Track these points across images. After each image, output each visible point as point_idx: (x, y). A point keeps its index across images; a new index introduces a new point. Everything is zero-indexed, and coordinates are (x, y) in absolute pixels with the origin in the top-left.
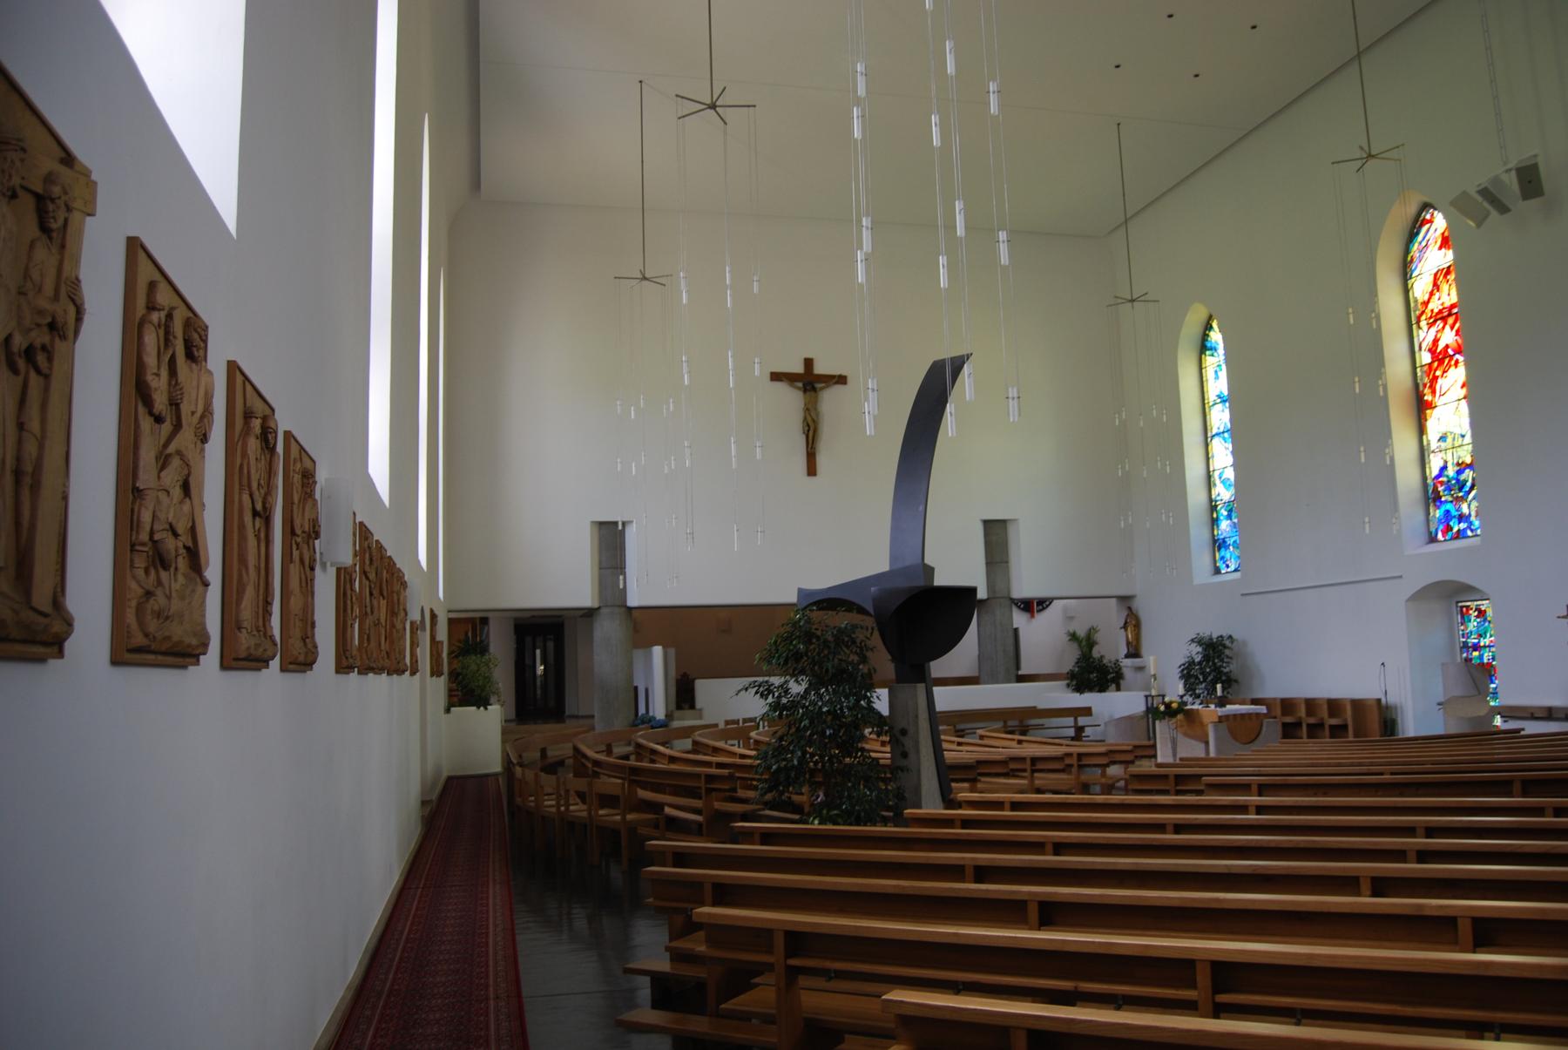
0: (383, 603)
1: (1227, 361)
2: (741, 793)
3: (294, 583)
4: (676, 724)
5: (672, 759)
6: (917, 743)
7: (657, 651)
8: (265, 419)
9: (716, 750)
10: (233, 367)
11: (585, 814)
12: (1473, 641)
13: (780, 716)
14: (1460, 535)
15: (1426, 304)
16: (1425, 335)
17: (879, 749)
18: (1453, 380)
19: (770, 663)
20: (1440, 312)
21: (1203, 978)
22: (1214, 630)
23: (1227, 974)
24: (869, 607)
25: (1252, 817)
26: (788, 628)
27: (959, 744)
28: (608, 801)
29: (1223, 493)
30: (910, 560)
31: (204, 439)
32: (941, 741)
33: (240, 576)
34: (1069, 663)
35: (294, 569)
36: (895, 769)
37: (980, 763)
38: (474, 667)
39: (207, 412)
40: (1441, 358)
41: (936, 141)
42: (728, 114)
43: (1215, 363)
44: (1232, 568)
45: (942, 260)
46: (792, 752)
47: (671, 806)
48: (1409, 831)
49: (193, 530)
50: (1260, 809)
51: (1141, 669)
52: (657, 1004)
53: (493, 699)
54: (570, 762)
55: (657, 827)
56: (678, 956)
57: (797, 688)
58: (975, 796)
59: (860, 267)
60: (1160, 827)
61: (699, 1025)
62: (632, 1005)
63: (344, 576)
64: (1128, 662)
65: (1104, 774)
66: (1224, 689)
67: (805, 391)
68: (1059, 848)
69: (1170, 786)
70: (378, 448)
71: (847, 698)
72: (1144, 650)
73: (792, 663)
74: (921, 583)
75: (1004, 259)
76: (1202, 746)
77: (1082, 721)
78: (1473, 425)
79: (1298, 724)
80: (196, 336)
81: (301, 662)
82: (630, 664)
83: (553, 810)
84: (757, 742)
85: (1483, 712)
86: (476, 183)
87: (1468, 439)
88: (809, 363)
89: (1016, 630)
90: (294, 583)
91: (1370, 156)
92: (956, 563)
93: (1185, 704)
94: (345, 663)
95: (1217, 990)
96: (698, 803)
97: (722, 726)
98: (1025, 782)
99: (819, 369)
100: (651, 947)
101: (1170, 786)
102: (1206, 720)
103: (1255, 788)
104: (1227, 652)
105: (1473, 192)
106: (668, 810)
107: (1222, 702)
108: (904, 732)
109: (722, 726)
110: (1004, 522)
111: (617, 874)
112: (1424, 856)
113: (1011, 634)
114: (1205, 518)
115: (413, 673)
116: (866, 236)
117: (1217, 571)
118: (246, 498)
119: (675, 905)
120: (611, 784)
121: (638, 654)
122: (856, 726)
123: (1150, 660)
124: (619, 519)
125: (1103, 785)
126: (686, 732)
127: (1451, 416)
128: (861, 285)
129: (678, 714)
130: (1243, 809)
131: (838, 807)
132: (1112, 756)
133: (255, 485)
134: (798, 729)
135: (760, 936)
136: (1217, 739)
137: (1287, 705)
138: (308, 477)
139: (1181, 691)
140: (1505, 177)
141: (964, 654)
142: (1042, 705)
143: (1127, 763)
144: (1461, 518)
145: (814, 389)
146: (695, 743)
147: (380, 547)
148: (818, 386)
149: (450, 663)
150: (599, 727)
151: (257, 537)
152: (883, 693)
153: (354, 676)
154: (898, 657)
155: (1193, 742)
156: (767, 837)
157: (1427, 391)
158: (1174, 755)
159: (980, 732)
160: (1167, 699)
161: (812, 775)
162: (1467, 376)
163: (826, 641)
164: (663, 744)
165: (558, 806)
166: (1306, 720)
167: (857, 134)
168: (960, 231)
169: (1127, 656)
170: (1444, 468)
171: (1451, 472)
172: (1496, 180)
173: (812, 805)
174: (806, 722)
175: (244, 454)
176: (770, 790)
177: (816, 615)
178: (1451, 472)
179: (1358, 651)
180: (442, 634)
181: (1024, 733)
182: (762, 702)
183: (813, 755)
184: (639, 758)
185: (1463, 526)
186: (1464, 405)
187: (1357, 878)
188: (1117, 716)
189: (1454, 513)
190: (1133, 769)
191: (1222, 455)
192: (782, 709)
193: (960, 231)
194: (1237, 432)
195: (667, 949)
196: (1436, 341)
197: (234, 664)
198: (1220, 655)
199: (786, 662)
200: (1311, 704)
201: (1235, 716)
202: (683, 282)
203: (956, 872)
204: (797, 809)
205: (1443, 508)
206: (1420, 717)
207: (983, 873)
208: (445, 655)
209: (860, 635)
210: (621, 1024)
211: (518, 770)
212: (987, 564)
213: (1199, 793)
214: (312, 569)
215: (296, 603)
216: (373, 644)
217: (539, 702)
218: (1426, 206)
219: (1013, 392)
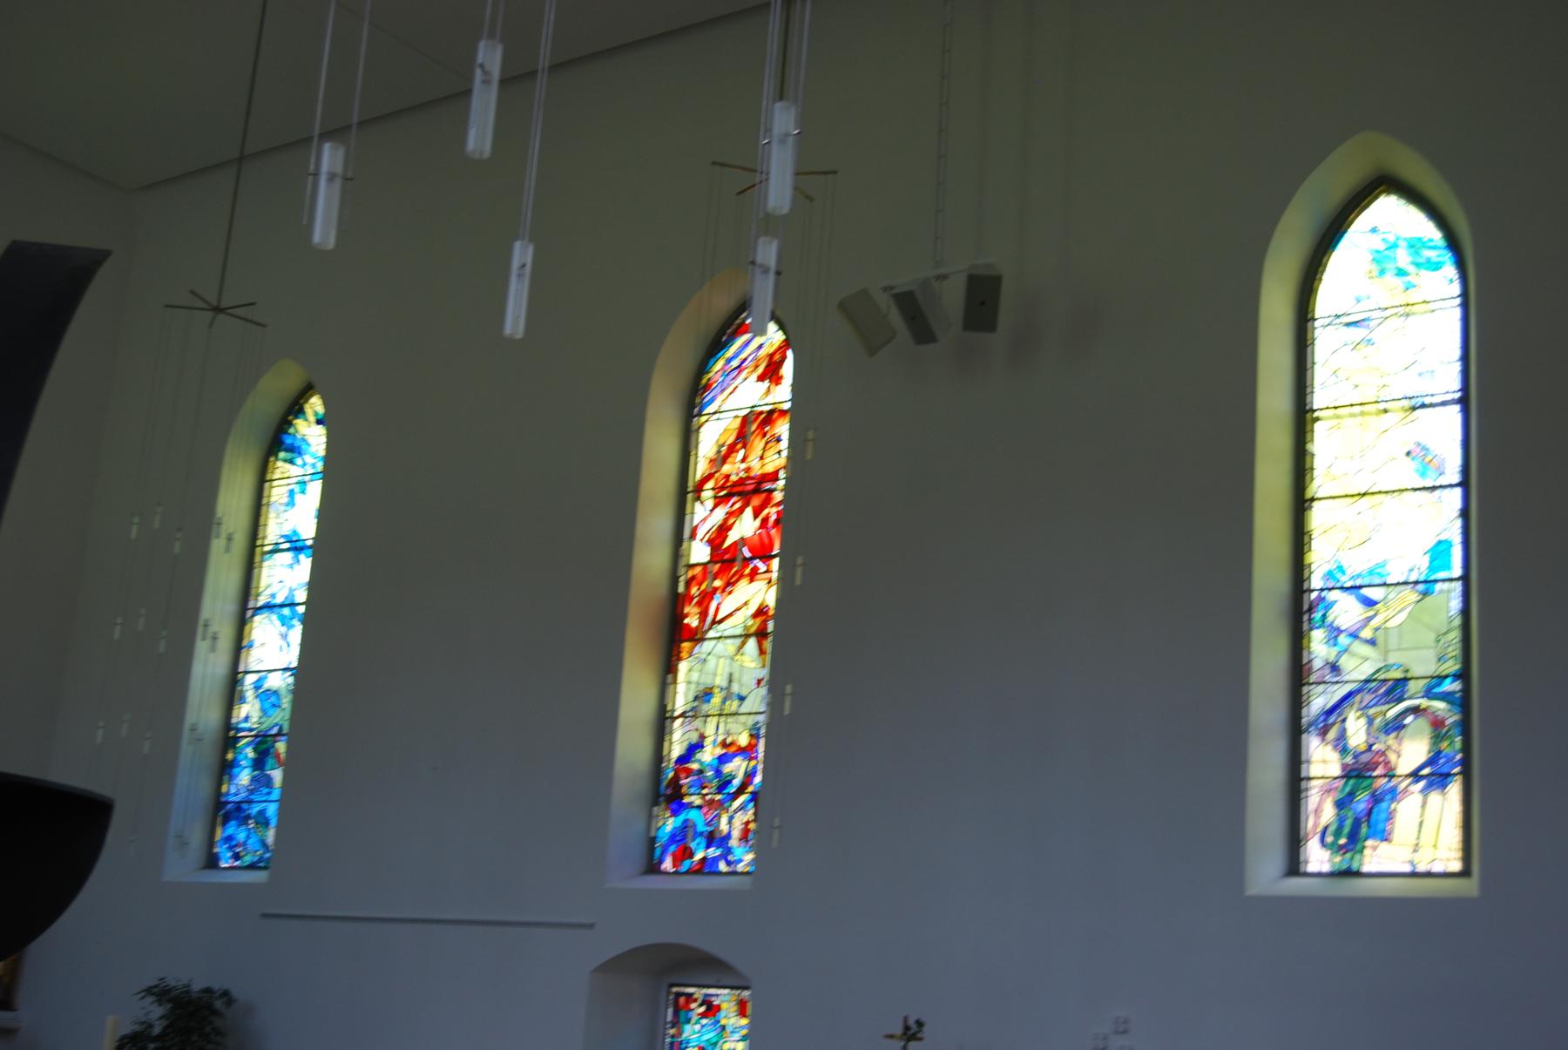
14: (706, 867)
16: (705, 514)
20: (741, 482)
22: (196, 975)
117: (212, 862)
144: (711, 839)
147: (187, 990)
170: (694, 748)
171: (708, 755)
194: (322, 616)
196: (724, 529)
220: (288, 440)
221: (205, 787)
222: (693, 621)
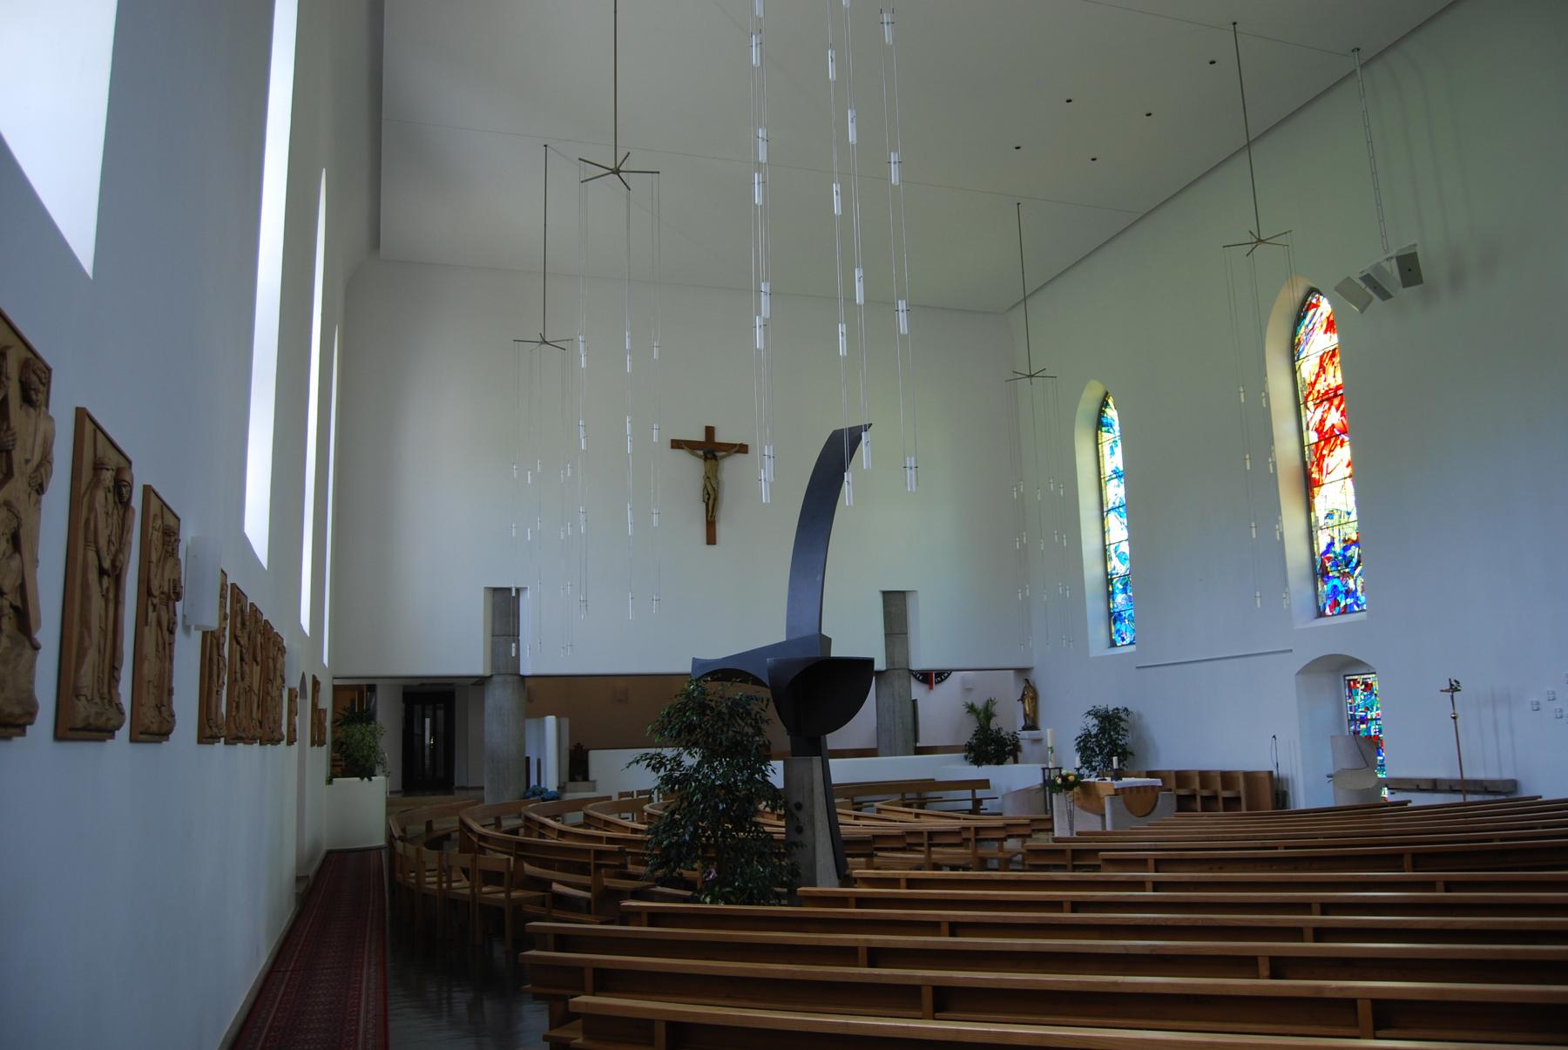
1: (1122, 436)
2: (632, 868)
3: (150, 648)
4: (569, 796)
5: (562, 834)
6: (812, 817)
7: (551, 721)
8: (119, 471)
9: (608, 824)
10: (82, 416)
12: (1359, 714)
13: (672, 789)
14: (1346, 610)
15: (1313, 384)
16: (1312, 416)
17: (774, 825)
18: (1339, 459)
19: (662, 734)
20: (1327, 392)
22: (1110, 703)
24: (766, 680)
25: (1149, 894)
26: (682, 699)
27: (857, 818)
28: (492, 877)
29: (1119, 567)
30: (807, 630)
31: (40, 489)
33: (82, 638)
34: (967, 735)
35: (150, 634)
37: (876, 837)
38: (358, 736)
39: (46, 460)
40: (1328, 437)
41: (837, 210)
42: (632, 179)
44: (1128, 641)
45: (842, 328)
46: (684, 827)
47: (559, 882)
48: (1305, 907)
49: (22, 589)
50: (1157, 886)
51: (1038, 741)
53: (378, 769)
55: (543, 905)
57: (690, 761)
58: (871, 873)
60: (1056, 905)
63: (211, 642)
64: (1026, 734)
65: (1001, 848)
66: (1119, 761)
67: (706, 459)
68: (955, 928)
69: (1066, 861)
70: (257, 504)
71: (741, 770)
72: (1041, 724)
73: (685, 735)
74: (818, 654)
75: (903, 328)
76: (1099, 818)
77: (980, 793)
78: (1357, 503)
79: (1192, 797)
80: (34, 378)
81: (154, 730)
82: (522, 735)
83: (435, 887)
84: (650, 815)
85: (1371, 785)
87: (1354, 516)
88: (710, 431)
90: (150, 648)
91: (1260, 241)
92: (853, 633)
93: (1082, 776)
94: (208, 732)
95: (1074, 859)
96: (586, 880)
99: (720, 438)
101: (1066, 861)
102: (1102, 793)
103: (1151, 864)
104: (1122, 724)
105: (1356, 278)
106: (556, 887)
107: (1118, 775)
109: (615, 798)
111: (499, 952)
112: (1321, 934)
113: (910, 706)
114: (1101, 592)
115: (291, 742)
116: (765, 301)
117: (1113, 644)
118: (92, 555)
119: (554, 991)
120: (496, 859)
121: (531, 724)
122: (750, 800)
123: (1047, 733)
124: (513, 585)
126: (578, 805)
127: (1337, 494)
128: (759, 351)
130: (1139, 885)
131: (731, 884)
132: (1009, 830)
133: (103, 542)
134: (690, 803)
136: (1114, 814)
137: (1182, 777)
138: (170, 535)
139: (1078, 764)
140: (1386, 265)
141: (862, 725)
142: (940, 778)
143: (1024, 837)
144: (1348, 593)
145: (715, 458)
146: (587, 816)
147: (255, 610)
148: (719, 454)
149: (334, 732)
150: (489, 800)
151: (105, 597)
152: (778, 765)
153: (220, 746)
154: (794, 728)
156: (655, 918)
157: (1314, 469)
158: (1071, 828)
159: (877, 805)
160: (1064, 772)
161: (705, 851)
162: (1352, 455)
163: (720, 713)
164: (554, 818)
165: (440, 882)
166: (1202, 792)
168: (859, 298)
169: (1024, 729)
170: (1331, 544)
171: (1338, 548)
172: (1378, 267)
175: (91, 508)
176: (660, 866)
177: (712, 687)
178: (1338, 548)
179: (1249, 723)
180: (326, 702)
181: (921, 806)
183: (705, 830)
184: (529, 832)
185: (1349, 601)
186: (1349, 482)
187: (1255, 958)
189: (1341, 588)
190: (1030, 843)
191: (1118, 530)
192: (674, 783)
193: (859, 298)
194: (1133, 508)
196: (1322, 421)
197: (71, 734)
198: (1116, 728)
199: (679, 734)
200: (1204, 776)
204: (688, 884)
205: (1331, 583)
206: (1311, 789)
207: (876, 956)
208: (328, 724)
209: (754, 707)
211: (399, 844)
212: (887, 635)
213: (1096, 868)
214: (172, 632)
215: (150, 669)
216: (242, 713)
217: (427, 772)
218: (1312, 291)
219: (910, 462)
221: (1102, 607)
222: (1315, 476)
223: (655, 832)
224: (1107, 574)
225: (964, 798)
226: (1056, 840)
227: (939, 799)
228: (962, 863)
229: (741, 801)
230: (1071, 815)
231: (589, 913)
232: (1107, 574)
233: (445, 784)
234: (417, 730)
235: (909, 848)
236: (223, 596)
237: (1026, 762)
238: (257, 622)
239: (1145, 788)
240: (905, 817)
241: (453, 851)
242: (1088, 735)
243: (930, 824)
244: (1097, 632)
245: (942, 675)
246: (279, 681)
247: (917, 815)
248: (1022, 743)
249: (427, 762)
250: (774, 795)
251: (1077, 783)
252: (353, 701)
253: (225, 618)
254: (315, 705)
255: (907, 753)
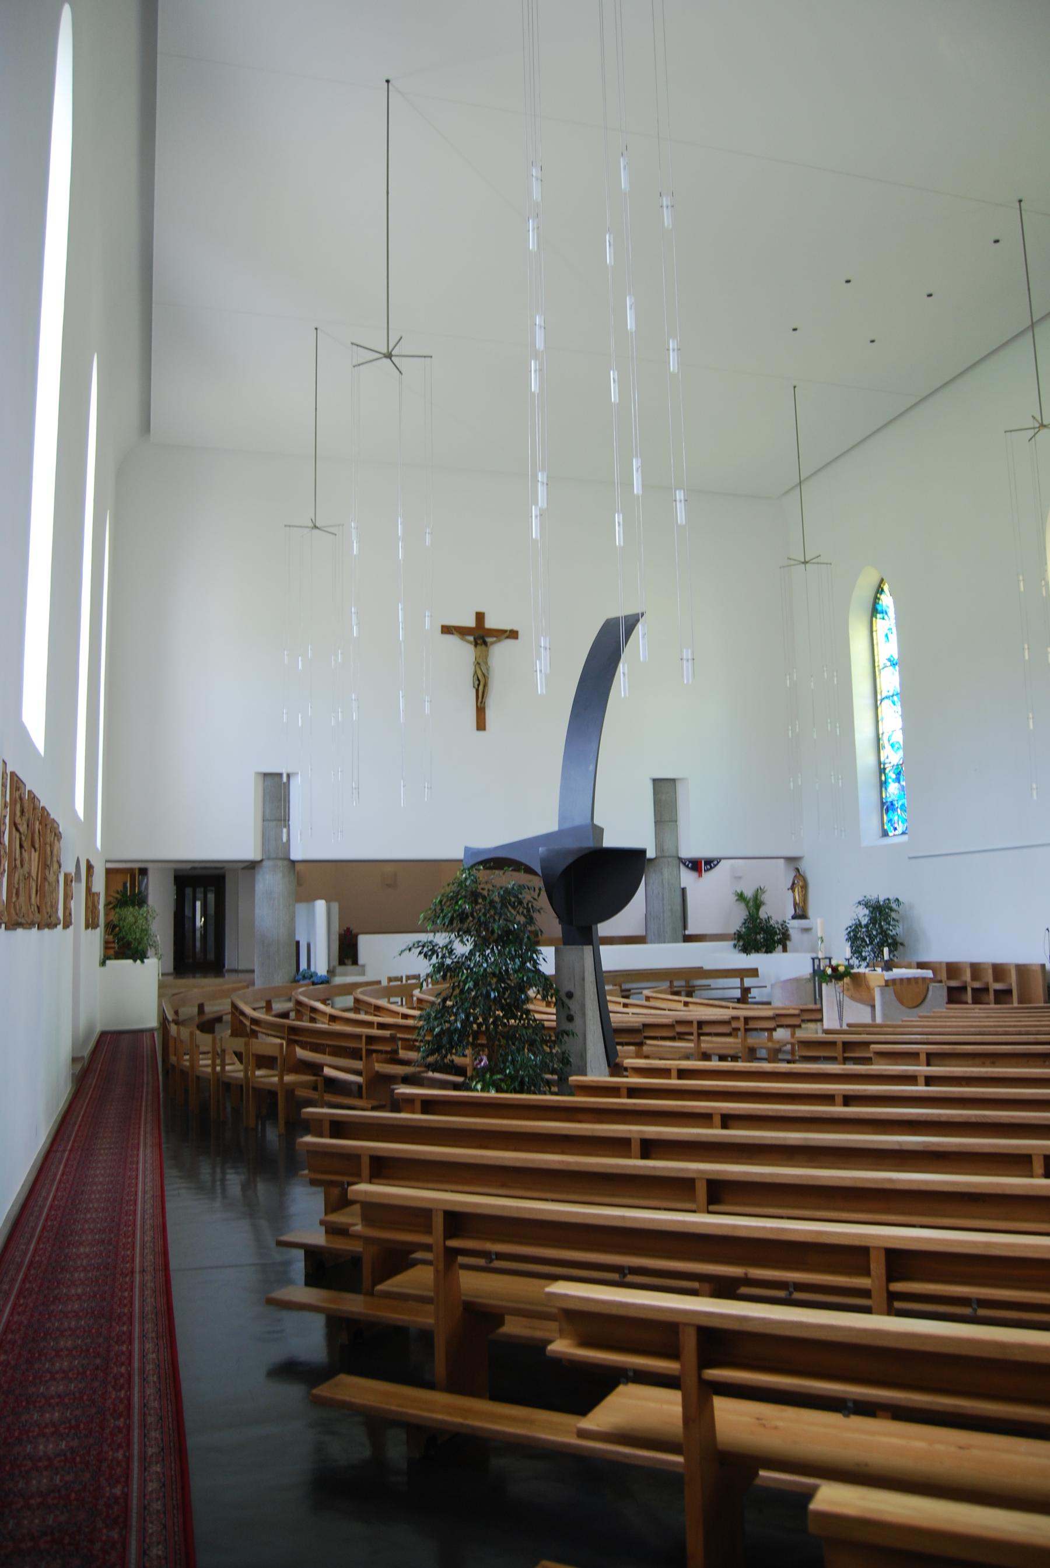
0: (35, 855)
2: (403, 1054)
4: (338, 980)
5: (333, 1018)
6: (583, 1006)
7: (321, 905)
9: (378, 1009)
11: (241, 1075)
17: (545, 1013)
21: (878, 1265)
22: (880, 893)
23: (901, 1262)
26: (455, 888)
27: (625, 1005)
28: (265, 1061)
29: (892, 757)
30: (579, 820)
32: (606, 1002)
34: (736, 920)
36: (560, 1034)
37: (646, 1026)
38: (131, 919)
41: (614, 398)
43: (885, 625)
44: (900, 830)
45: (618, 518)
46: (456, 1015)
50: (929, 1080)
52: (312, 1280)
53: (150, 952)
54: (227, 1018)
55: (315, 1089)
56: (333, 1230)
57: (462, 948)
59: (535, 522)
60: (828, 1099)
61: (354, 1304)
62: (285, 1280)
64: (796, 923)
65: (770, 1038)
66: (890, 952)
67: (476, 644)
68: (727, 1120)
69: (838, 1053)
71: (512, 959)
72: (811, 911)
74: (590, 844)
75: (681, 518)
76: (868, 1009)
77: (748, 982)
79: (963, 989)
82: (292, 919)
83: (209, 1070)
86: (146, 426)
88: (480, 617)
89: (684, 890)
92: (625, 827)
93: (852, 967)
95: (891, 1278)
96: (358, 1065)
97: (385, 983)
98: (691, 1045)
99: (490, 623)
100: (307, 1214)
104: (893, 915)
106: (327, 1071)
107: (888, 966)
108: (570, 995)
110: (673, 781)
111: (273, 1135)
113: (679, 893)
115: (66, 926)
116: (541, 491)
117: (885, 834)
120: (270, 1043)
121: (301, 908)
122: (522, 988)
123: (817, 921)
125: (769, 1050)
126: (348, 989)
129: (340, 969)
130: (911, 1079)
131: (502, 1071)
132: (779, 1020)
134: (462, 991)
135: (418, 1216)
136: (884, 1004)
137: (953, 969)
141: (630, 918)
142: (708, 966)
145: (485, 643)
146: (357, 1001)
147: (33, 798)
148: (489, 640)
149: (106, 915)
150: (259, 984)
154: (566, 916)
155: (859, 1005)
156: (428, 1105)
158: (841, 1018)
159: (646, 992)
160: (834, 963)
161: (475, 1038)
163: (492, 902)
164: (324, 1002)
165: (214, 1065)
166: (970, 985)
167: (534, 387)
168: (637, 489)
169: (794, 917)
173: (475, 1069)
174: (470, 984)
176: (432, 1053)
177: (482, 874)
180: (99, 885)
181: (689, 994)
182: (426, 961)
184: (299, 1016)
188: (784, 978)
190: (800, 1034)
193: (637, 489)
194: (907, 697)
195: (322, 1223)
199: (451, 922)
200: (976, 969)
201: (901, 980)
202: (354, 532)
203: (620, 1146)
204: (460, 1071)
207: (649, 1148)
208: (101, 907)
209: (526, 896)
210: (271, 1302)
213: (867, 1061)
216: (22, 898)
217: (199, 953)
219: (687, 654)
220: (879, 608)
223: (427, 1018)
224: (880, 763)
225: (732, 987)
226: (827, 1032)
227: (708, 987)
228: (732, 1052)
229: (510, 990)
230: (840, 1006)
231: (361, 1097)
232: (880, 763)
233: (214, 966)
234: (188, 912)
235: (680, 1037)
236: (4, 785)
237: (795, 951)
238: (34, 809)
239: (916, 980)
240: (673, 1005)
241: (224, 1032)
242: (859, 925)
243: (699, 1013)
244: (870, 821)
245: (711, 863)
246: (56, 866)
247: (686, 1004)
248: (791, 932)
249: (198, 944)
250: (546, 984)
251: (847, 973)
252: (125, 884)
253: (5, 807)
254: (88, 889)
255: (675, 941)
